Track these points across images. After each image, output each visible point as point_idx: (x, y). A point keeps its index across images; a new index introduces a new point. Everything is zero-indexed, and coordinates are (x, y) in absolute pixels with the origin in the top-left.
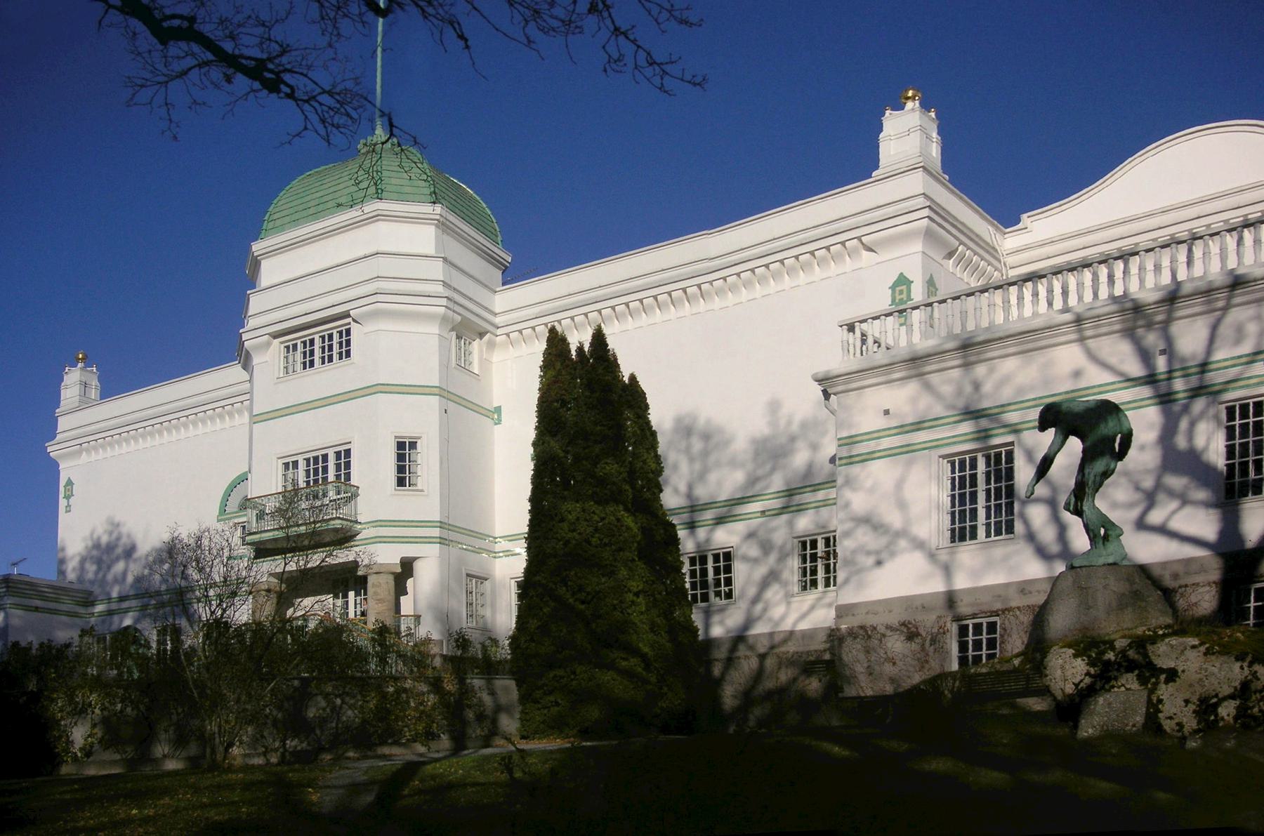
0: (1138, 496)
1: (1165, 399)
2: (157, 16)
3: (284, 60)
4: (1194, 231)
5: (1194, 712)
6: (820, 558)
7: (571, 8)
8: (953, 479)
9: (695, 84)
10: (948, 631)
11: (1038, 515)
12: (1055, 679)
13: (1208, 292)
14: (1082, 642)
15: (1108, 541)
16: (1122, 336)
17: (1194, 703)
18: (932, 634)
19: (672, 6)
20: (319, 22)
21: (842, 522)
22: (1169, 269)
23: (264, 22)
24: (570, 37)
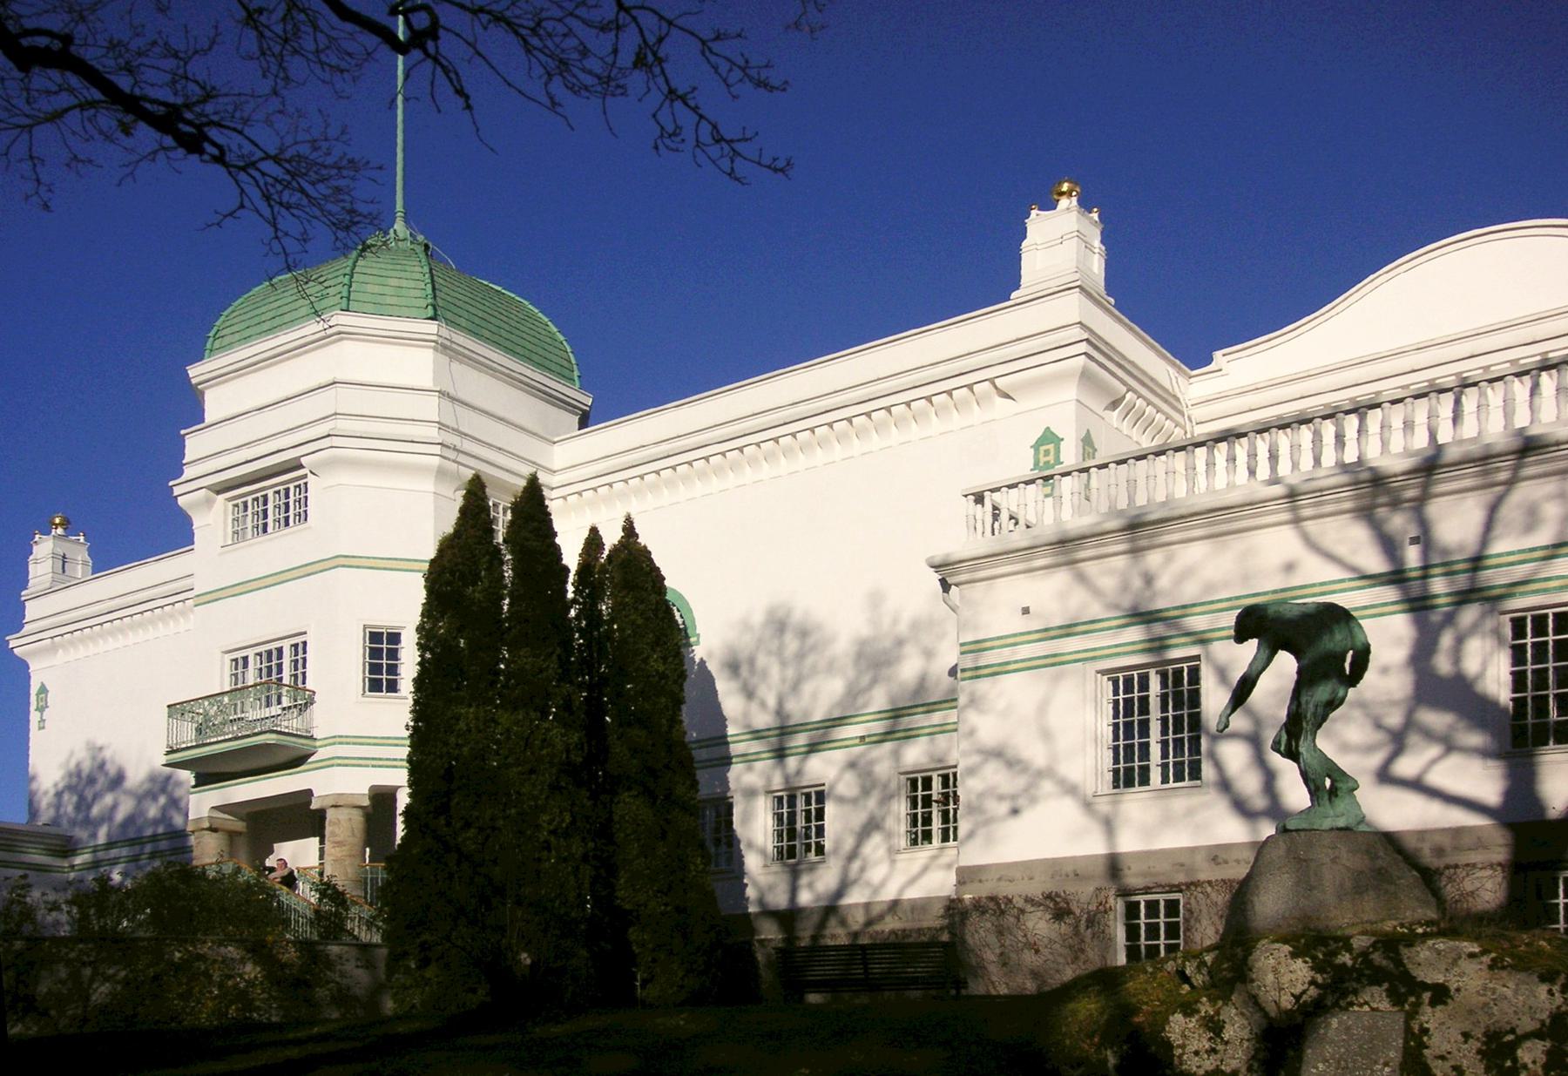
0: (1379, 736)
1: (1418, 605)
2: (10, 28)
3: (209, 108)
4: (1465, 375)
5: (1479, 1052)
6: (936, 801)
7: (610, 60)
8: (1116, 703)
9: (776, 170)
10: (1111, 909)
11: (1235, 756)
12: (1265, 986)
13: (1484, 459)
14: (1303, 936)
15: (1337, 796)
17: (1478, 1039)
18: (1088, 913)
19: (747, 62)
20: (258, 58)
21: (965, 754)
22: (1426, 426)
23: (177, 52)
24: (609, 100)
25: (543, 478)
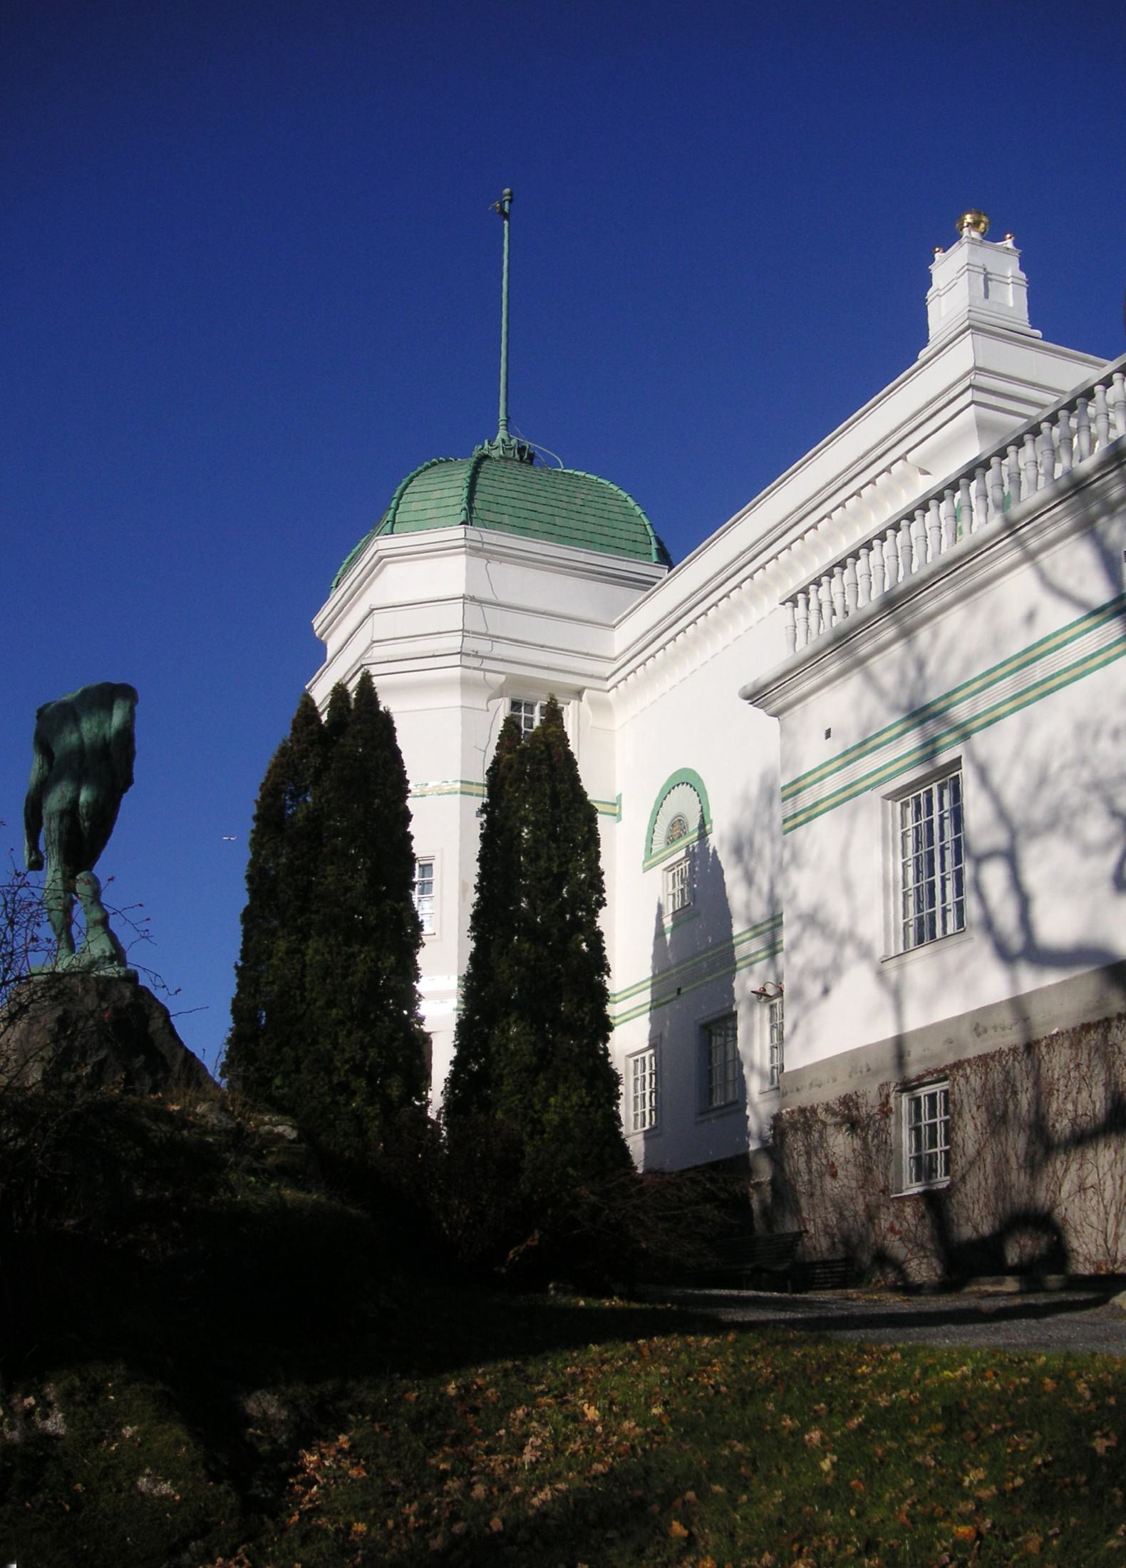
16: (1083, 536)
25: (374, 670)
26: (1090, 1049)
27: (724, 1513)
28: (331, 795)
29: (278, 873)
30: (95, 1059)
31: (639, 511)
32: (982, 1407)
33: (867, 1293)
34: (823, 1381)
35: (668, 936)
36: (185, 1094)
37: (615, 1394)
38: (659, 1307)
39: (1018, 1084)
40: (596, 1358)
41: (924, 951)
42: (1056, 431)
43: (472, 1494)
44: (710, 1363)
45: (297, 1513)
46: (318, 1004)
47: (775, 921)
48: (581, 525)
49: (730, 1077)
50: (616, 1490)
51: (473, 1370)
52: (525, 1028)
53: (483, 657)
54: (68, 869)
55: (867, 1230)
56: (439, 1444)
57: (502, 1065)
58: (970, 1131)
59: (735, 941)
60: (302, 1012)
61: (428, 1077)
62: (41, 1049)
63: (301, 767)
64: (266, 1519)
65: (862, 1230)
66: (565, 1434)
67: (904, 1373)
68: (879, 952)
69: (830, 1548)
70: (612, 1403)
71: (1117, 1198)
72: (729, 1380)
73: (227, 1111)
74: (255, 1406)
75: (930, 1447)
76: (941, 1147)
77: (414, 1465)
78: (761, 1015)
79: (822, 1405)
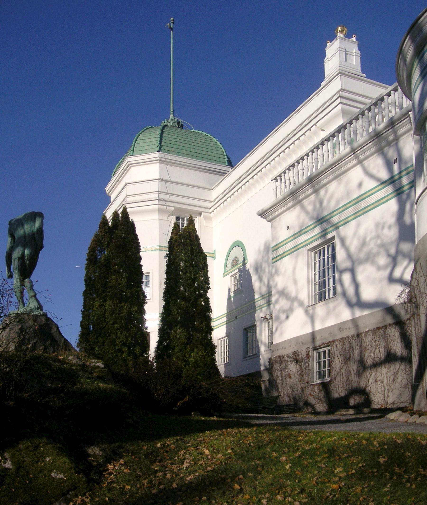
16: (379, 154)
25: (127, 206)
26: (380, 336)
27: (253, 482)
28: (113, 251)
29: (95, 279)
30: (33, 342)
31: (221, 146)
32: (341, 449)
33: (302, 415)
34: (287, 442)
35: (232, 299)
36: (65, 354)
37: (215, 446)
38: (230, 420)
39: (354, 347)
40: (208, 435)
41: (321, 304)
42: (370, 114)
43: (166, 477)
44: (247, 437)
45: (106, 483)
46: (110, 323)
47: (270, 294)
48: (200, 152)
49: (254, 346)
50: (215, 475)
51: (166, 439)
52: (182, 330)
53: (166, 201)
54: (22, 278)
55: (302, 395)
56: (155, 462)
57: (175, 342)
58: (337, 363)
59: (255, 301)
60: (105, 325)
61: (149, 346)
62: (14, 339)
63: (102, 241)
64: (95, 485)
65: (300, 395)
66: (198, 459)
67: (314, 439)
68: (306, 304)
69: (289, 492)
70: (214, 449)
71: (388, 384)
72: (254, 442)
73: (79, 358)
74: (91, 451)
75: (323, 462)
76: (327, 368)
77: (146, 468)
78: (265, 325)
79: (286, 449)
